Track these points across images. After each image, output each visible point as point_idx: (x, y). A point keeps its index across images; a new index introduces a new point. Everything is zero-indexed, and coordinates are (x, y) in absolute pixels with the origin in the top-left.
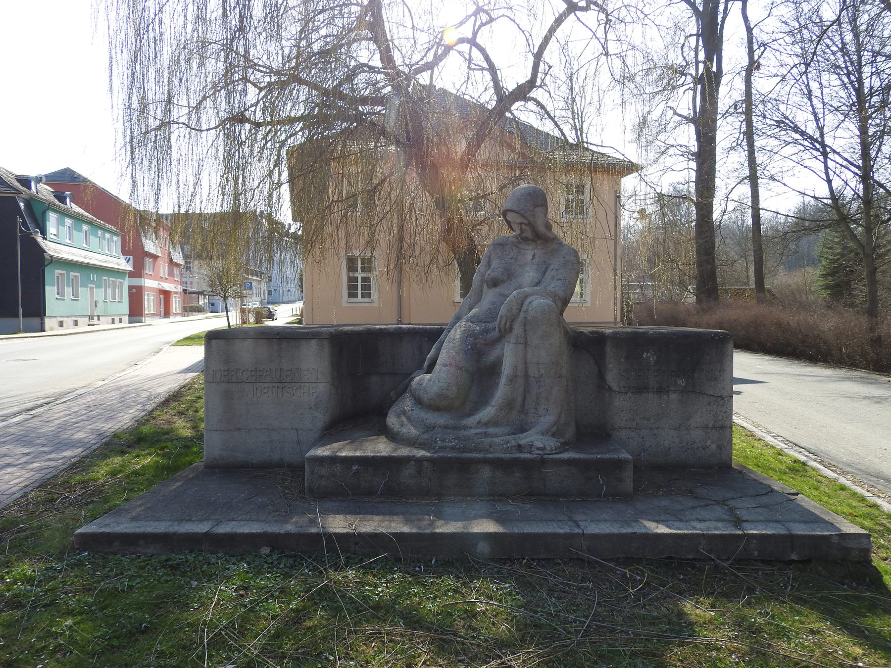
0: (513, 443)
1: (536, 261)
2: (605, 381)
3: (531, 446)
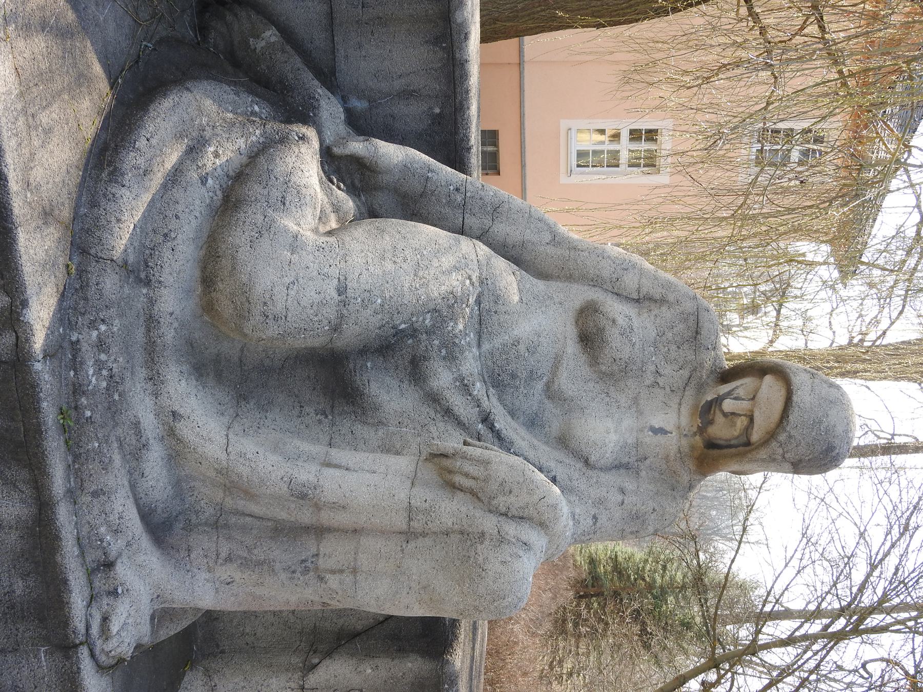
0: (115, 546)
1: (649, 438)
2: (329, 654)
3: (114, 593)
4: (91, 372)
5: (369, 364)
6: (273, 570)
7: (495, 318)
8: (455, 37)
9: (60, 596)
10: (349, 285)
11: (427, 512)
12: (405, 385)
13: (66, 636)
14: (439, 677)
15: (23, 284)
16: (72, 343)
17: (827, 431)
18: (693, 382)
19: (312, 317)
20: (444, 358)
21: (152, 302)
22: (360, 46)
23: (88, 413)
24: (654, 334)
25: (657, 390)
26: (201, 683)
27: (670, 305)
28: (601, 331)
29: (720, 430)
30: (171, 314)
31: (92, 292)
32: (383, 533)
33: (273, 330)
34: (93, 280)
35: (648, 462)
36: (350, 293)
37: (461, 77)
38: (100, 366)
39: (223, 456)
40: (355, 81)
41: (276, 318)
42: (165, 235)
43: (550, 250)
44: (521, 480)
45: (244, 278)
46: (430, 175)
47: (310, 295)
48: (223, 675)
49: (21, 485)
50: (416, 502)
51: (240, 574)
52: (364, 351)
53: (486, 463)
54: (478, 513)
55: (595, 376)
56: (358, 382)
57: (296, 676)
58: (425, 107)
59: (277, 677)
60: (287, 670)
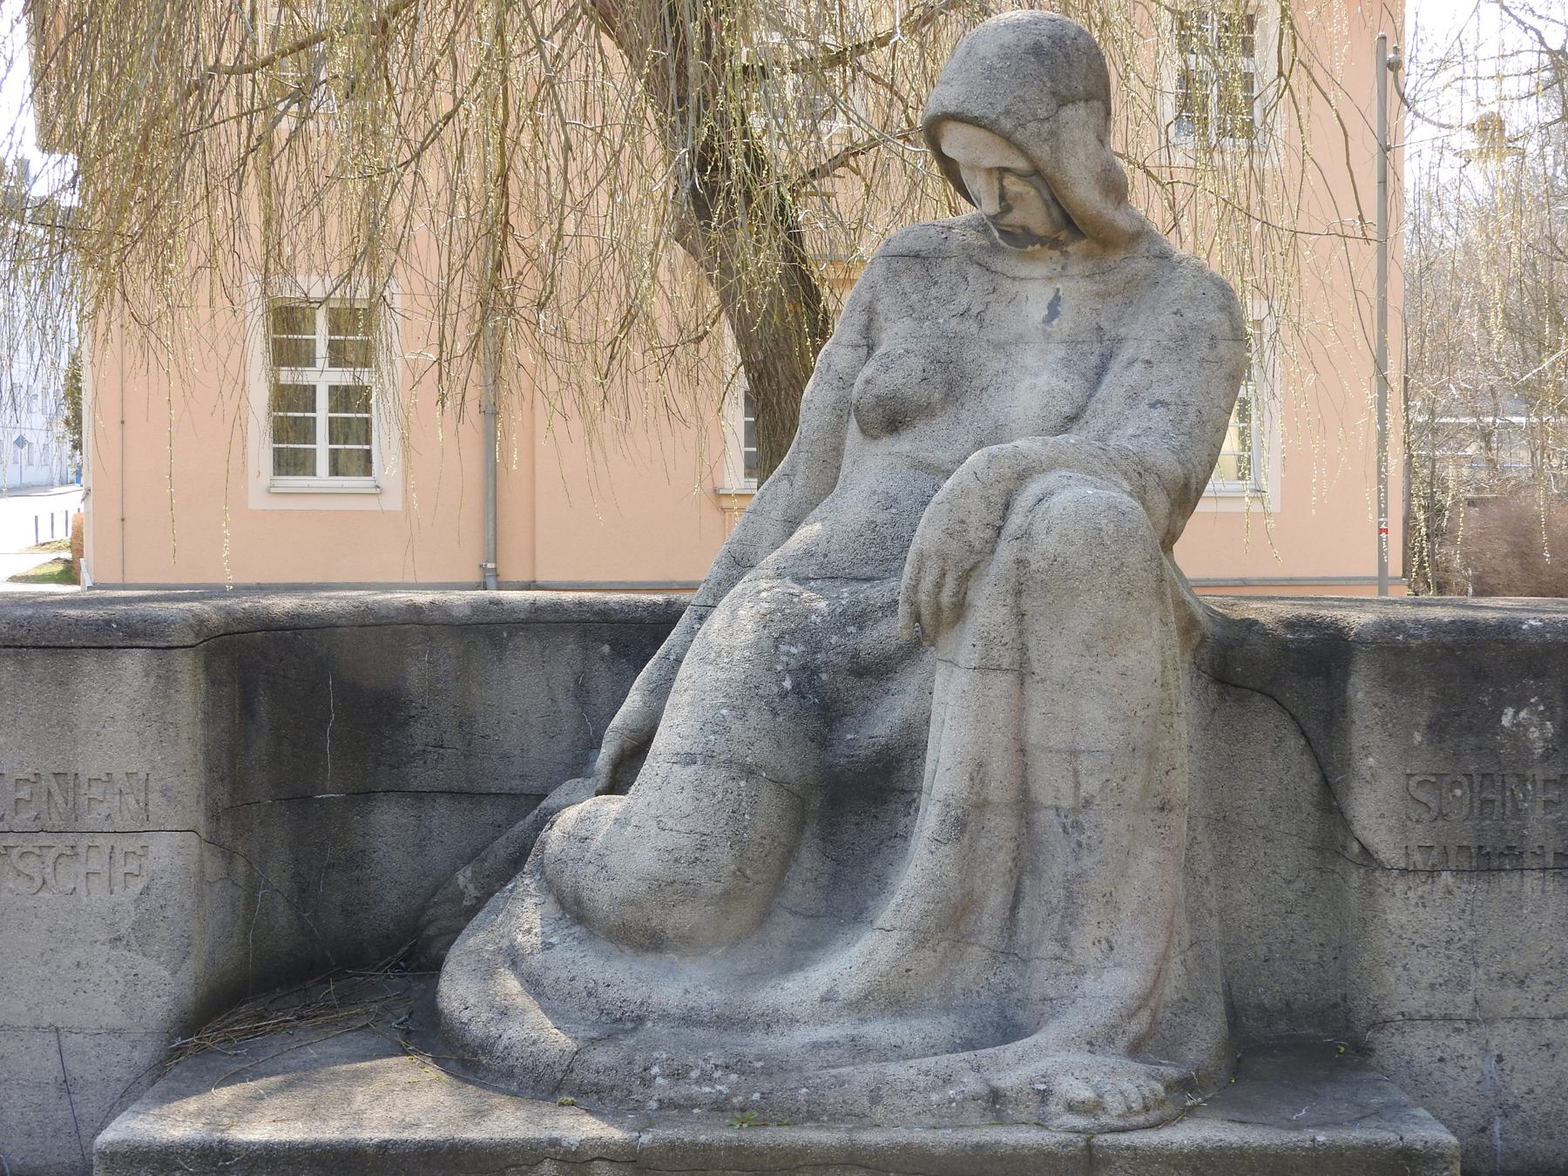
2: (1347, 824)
3: (1044, 1096)
4: (707, 1089)
5: (849, 737)
6: (1079, 876)
7: (832, 557)
8: (492, 618)
9: (1002, 1159)
10: (687, 749)
11: (988, 644)
12: (893, 686)
14: (1381, 648)
15: (528, 1141)
16: (660, 1108)
17: (1007, 57)
18: (986, 259)
19: (715, 801)
20: (861, 628)
21: (665, 1016)
22: (505, 756)
23: (756, 1096)
24: (908, 321)
25: (988, 316)
26: (1397, 1038)
27: (875, 299)
28: (880, 401)
30: (687, 991)
31: (604, 1079)
32: (1020, 711)
33: (724, 857)
34: (592, 1077)
35: (1105, 325)
36: (697, 749)
37: (557, 611)
38: (706, 1078)
39: (896, 935)
40: (561, 767)
41: (702, 848)
42: (590, 994)
43: (799, 481)
44: (947, 506)
45: (643, 887)
46: (672, 658)
47: (683, 801)
48: (1383, 999)
51: (1087, 928)
52: (823, 742)
53: (922, 558)
55: (951, 409)
56: (868, 752)
57: (1383, 881)
58: (601, 667)
59: (1384, 912)
60: (1371, 894)
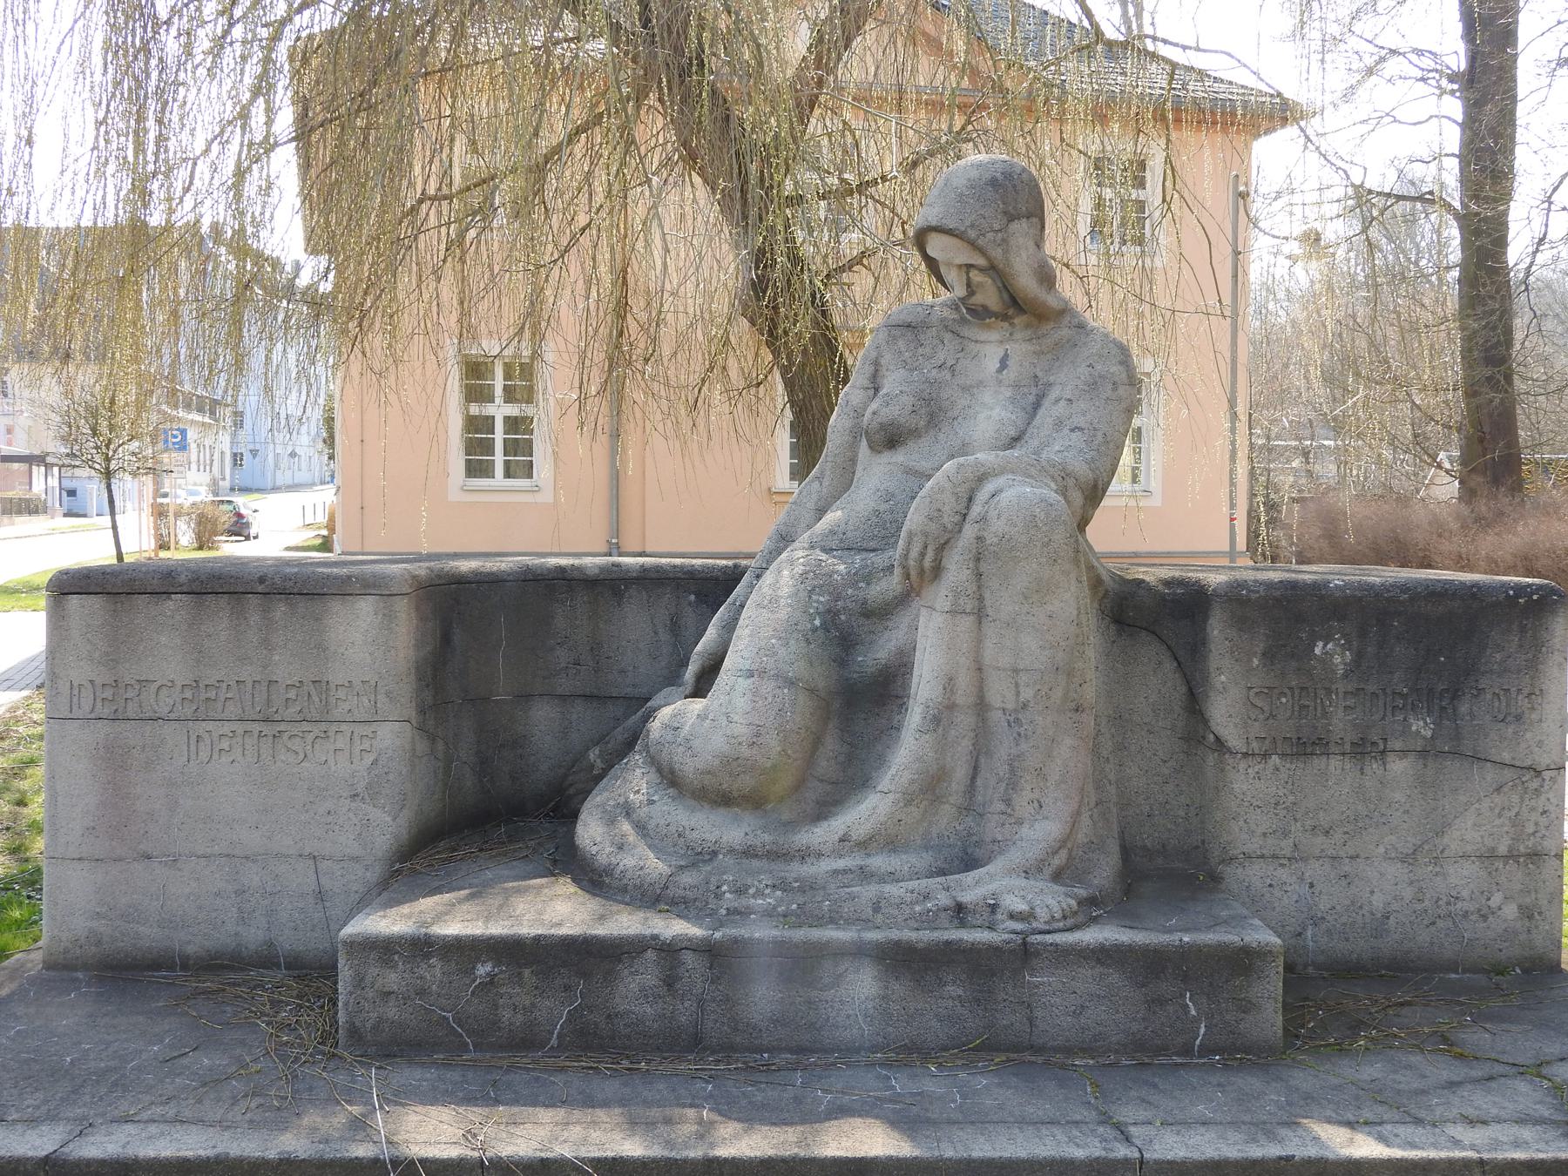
0: (943, 899)
1: (1010, 375)
3: (994, 908)
7: (849, 534)
11: (957, 595)
13: (1012, 951)
18: (957, 328)
21: (731, 851)
22: (622, 671)
25: (958, 368)
27: (880, 356)
28: (882, 426)
29: (989, 296)
32: (979, 642)
33: (773, 742)
34: (681, 892)
35: (1040, 374)
38: (759, 894)
39: (891, 796)
41: (758, 735)
43: (826, 482)
45: (717, 762)
49: (841, 969)
50: (947, 606)
52: (842, 662)
53: (911, 535)
54: (960, 544)
55: (932, 432)
57: (1231, 761)
